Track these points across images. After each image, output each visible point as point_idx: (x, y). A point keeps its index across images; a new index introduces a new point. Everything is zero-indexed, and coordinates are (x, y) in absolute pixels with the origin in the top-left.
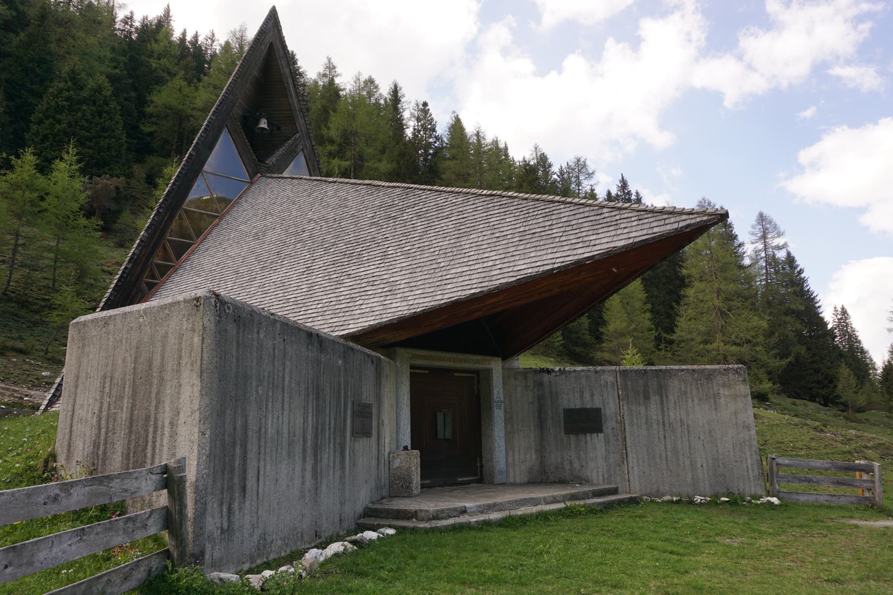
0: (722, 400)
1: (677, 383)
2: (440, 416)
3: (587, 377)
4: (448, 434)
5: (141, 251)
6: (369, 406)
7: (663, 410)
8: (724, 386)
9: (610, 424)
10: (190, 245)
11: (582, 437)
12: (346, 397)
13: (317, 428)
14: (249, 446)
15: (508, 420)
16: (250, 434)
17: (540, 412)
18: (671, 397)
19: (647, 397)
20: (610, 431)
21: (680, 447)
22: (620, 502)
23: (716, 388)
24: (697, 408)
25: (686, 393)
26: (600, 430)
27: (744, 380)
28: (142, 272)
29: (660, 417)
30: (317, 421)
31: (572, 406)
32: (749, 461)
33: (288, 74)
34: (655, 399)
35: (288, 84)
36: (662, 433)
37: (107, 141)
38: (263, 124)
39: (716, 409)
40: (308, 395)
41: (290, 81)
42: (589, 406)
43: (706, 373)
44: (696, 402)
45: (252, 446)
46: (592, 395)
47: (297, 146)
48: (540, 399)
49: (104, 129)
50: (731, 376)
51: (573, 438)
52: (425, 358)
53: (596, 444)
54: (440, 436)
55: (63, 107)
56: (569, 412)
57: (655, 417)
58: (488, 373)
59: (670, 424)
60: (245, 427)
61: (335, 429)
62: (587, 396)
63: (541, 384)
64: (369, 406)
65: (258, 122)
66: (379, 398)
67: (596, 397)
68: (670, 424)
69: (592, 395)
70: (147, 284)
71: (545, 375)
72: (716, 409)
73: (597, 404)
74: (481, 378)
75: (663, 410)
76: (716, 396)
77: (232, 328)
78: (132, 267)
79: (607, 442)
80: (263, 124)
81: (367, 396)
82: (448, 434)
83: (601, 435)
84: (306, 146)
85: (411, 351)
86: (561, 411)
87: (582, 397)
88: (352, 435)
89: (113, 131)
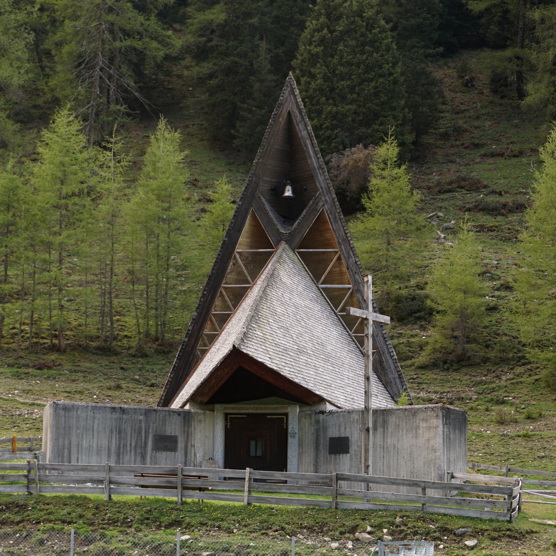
0: (421, 431)
1: (394, 419)
3: (344, 416)
4: (259, 453)
5: (193, 327)
7: (384, 438)
8: (423, 420)
9: (353, 448)
10: (229, 315)
11: (338, 456)
12: (147, 432)
13: (119, 446)
14: (72, 450)
15: (301, 445)
16: (72, 446)
17: (317, 440)
18: (390, 429)
20: (353, 452)
21: (391, 463)
23: (418, 421)
24: (405, 437)
25: (399, 425)
26: (347, 452)
27: (437, 416)
28: (196, 343)
29: (382, 443)
30: (120, 443)
31: (334, 436)
32: (433, 475)
35: (306, 146)
36: (382, 454)
37: (373, 84)
39: (416, 437)
40: (112, 432)
42: (343, 436)
43: (413, 411)
44: (404, 432)
45: (74, 450)
46: (345, 428)
47: (317, 204)
48: (317, 431)
49: (369, 69)
50: (429, 413)
51: (333, 456)
52: (233, 408)
53: (345, 459)
54: (253, 453)
55: (317, 55)
56: (332, 440)
57: (379, 443)
59: (387, 447)
60: (70, 443)
61: (136, 446)
62: (342, 428)
63: (318, 422)
67: (347, 429)
68: (387, 447)
69: (345, 428)
71: (321, 415)
72: (416, 437)
73: (348, 434)
75: (384, 438)
76: (417, 428)
77: (62, 413)
78: (189, 340)
79: (351, 459)
82: (259, 453)
83: (348, 455)
84: (326, 201)
85: (224, 405)
86: (328, 439)
88: (153, 450)
89: (381, 67)
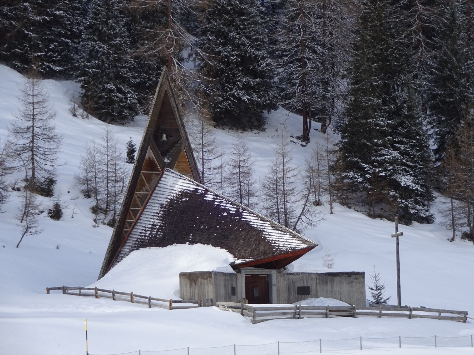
2: (255, 290)
6: (235, 288)
19: (327, 283)
22: (299, 237)
31: (300, 286)
33: (175, 106)
34: (329, 283)
38: (164, 138)
41: (176, 109)
42: (306, 286)
54: (255, 296)
58: (271, 275)
64: (235, 288)
65: (162, 137)
66: (237, 285)
70: (128, 222)
73: (309, 285)
74: (269, 276)
75: (332, 287)
80: (164, 138)
81: (234, 285)
82: (257, 295)
84: (186, 145)
86: (296, 287)
87: (303, 283)
